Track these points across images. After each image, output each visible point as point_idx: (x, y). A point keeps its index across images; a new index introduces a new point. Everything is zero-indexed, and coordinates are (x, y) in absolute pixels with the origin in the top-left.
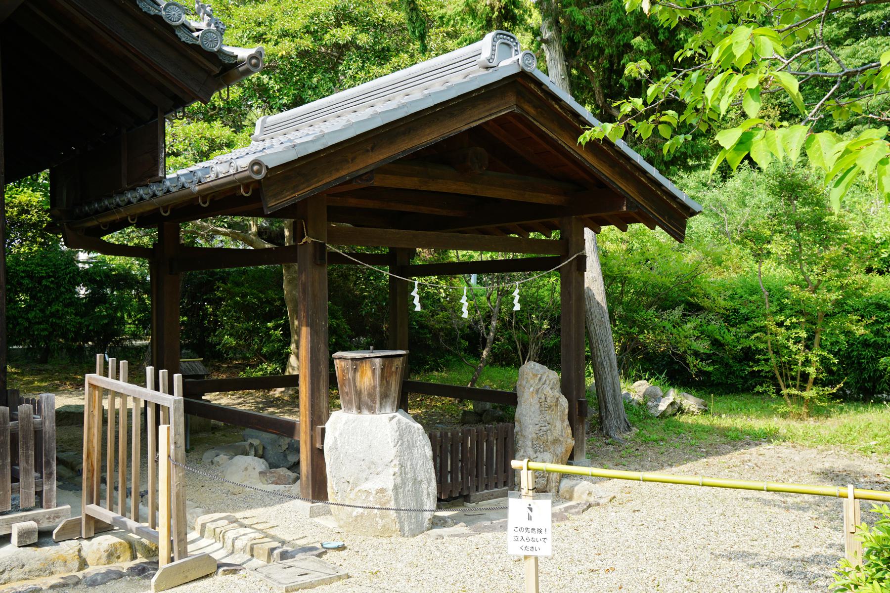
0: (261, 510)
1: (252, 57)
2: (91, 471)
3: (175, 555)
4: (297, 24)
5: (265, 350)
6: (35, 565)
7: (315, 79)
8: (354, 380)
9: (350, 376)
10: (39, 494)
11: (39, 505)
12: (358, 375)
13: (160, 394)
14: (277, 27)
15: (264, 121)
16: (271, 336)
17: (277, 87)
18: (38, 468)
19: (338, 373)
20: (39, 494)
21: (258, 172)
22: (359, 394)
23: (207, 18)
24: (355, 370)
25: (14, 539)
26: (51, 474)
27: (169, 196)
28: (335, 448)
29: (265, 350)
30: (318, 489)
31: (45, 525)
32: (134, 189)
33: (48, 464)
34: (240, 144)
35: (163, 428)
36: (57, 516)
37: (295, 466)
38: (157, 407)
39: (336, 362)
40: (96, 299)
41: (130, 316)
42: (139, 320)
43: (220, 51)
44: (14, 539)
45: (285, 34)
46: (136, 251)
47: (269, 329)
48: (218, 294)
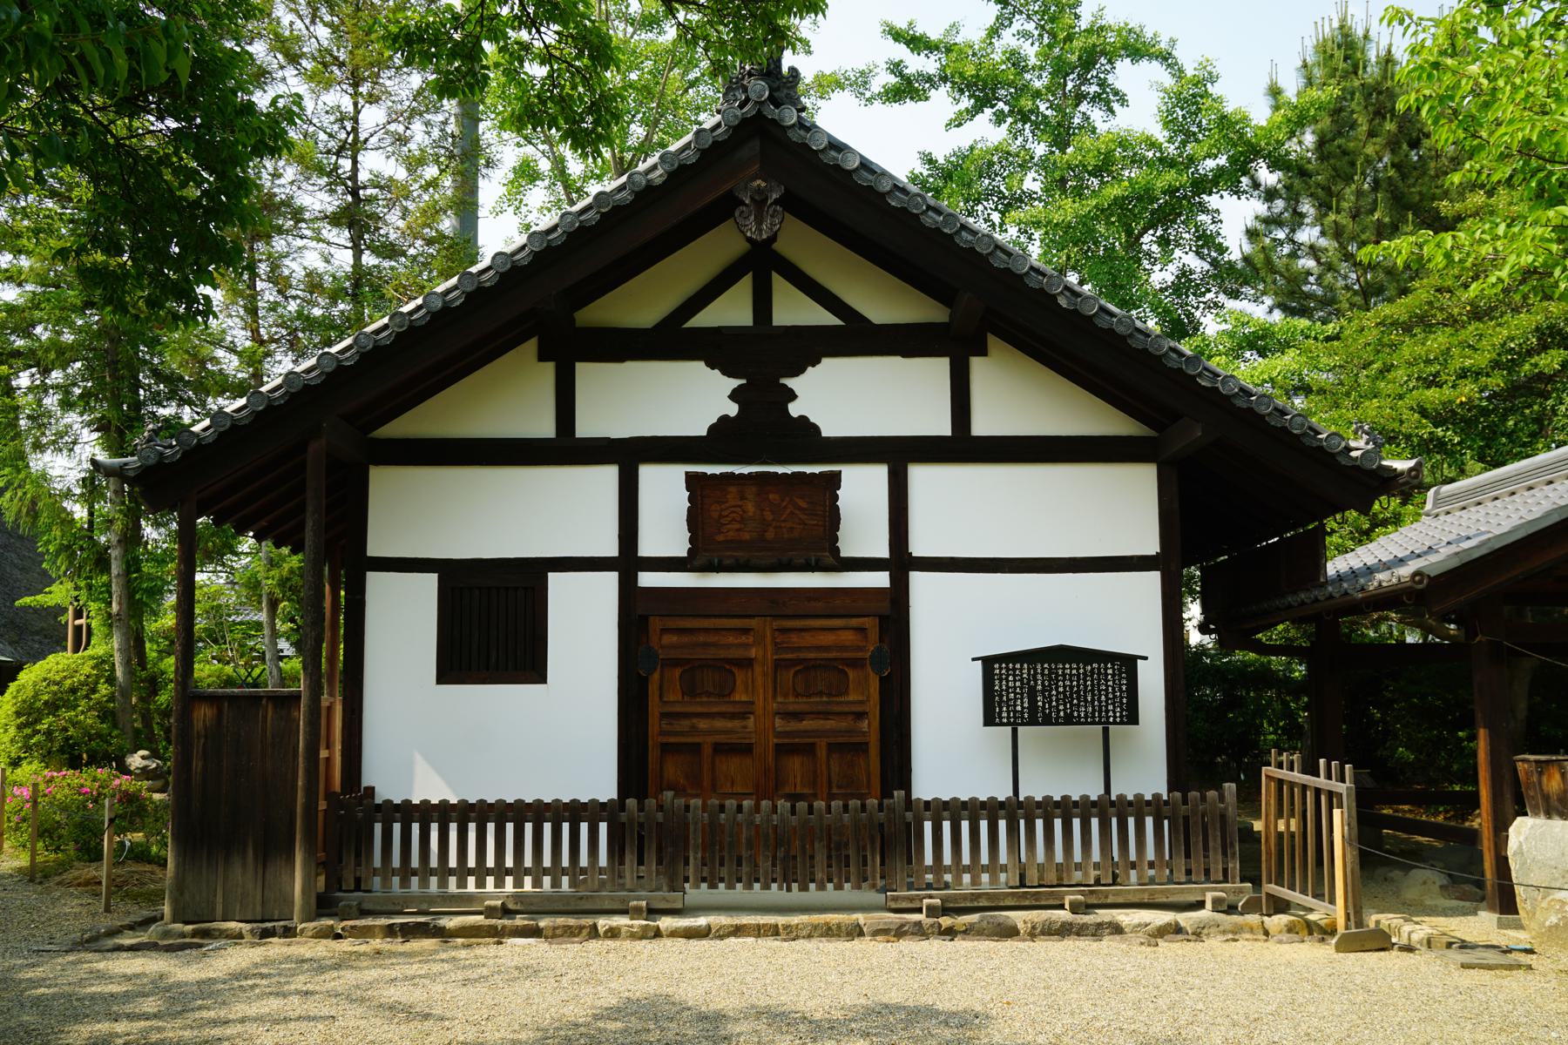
0: (1442, 919)
1: (1411, 470)
2: (1269, 853)
3: (1352, 923)
4: (1482, 359)
5: (1455, 767)
6: (1228, 927)
7: (1511, 423)
8: (1540, 783)
9: (1535, 779)
10: (1225, 871)
11: (1226, 881)
12: (1545, 779)
13: (1333, 782)
14: (1456, 364)
15: (1437, 493)
16: (1463, 749)
17: (1457, 440)
18: (1225, 854)
19: (1522, 775)
20: (1225, 871)
21: (1421, 582)
22: (1546, 798)
23: (1365, 437)
24: (1541, 774)
25: (1209, 905)
26: (1234, 854)
27: (1332, 602)
28: (1520, 852)
29: (1455, 767)
30: (1506, 902)
31: (1232, 898)
32: (1295, 593)
33: (1232, 845)
34: (1408, 519)
35: (1337, 813)
36: (1241, 891)
37: (1480, 884)
38: (1330, 794)
39: (1519, 765)
40: (1231, 702)
41: (1270, 724)
42: (1283, 728)
43: (1381, 467)
44: (1209, 905)
45: (1463, 374)
46: (1287, 649)
47: (1462, 740)
48: (1388, 695)
